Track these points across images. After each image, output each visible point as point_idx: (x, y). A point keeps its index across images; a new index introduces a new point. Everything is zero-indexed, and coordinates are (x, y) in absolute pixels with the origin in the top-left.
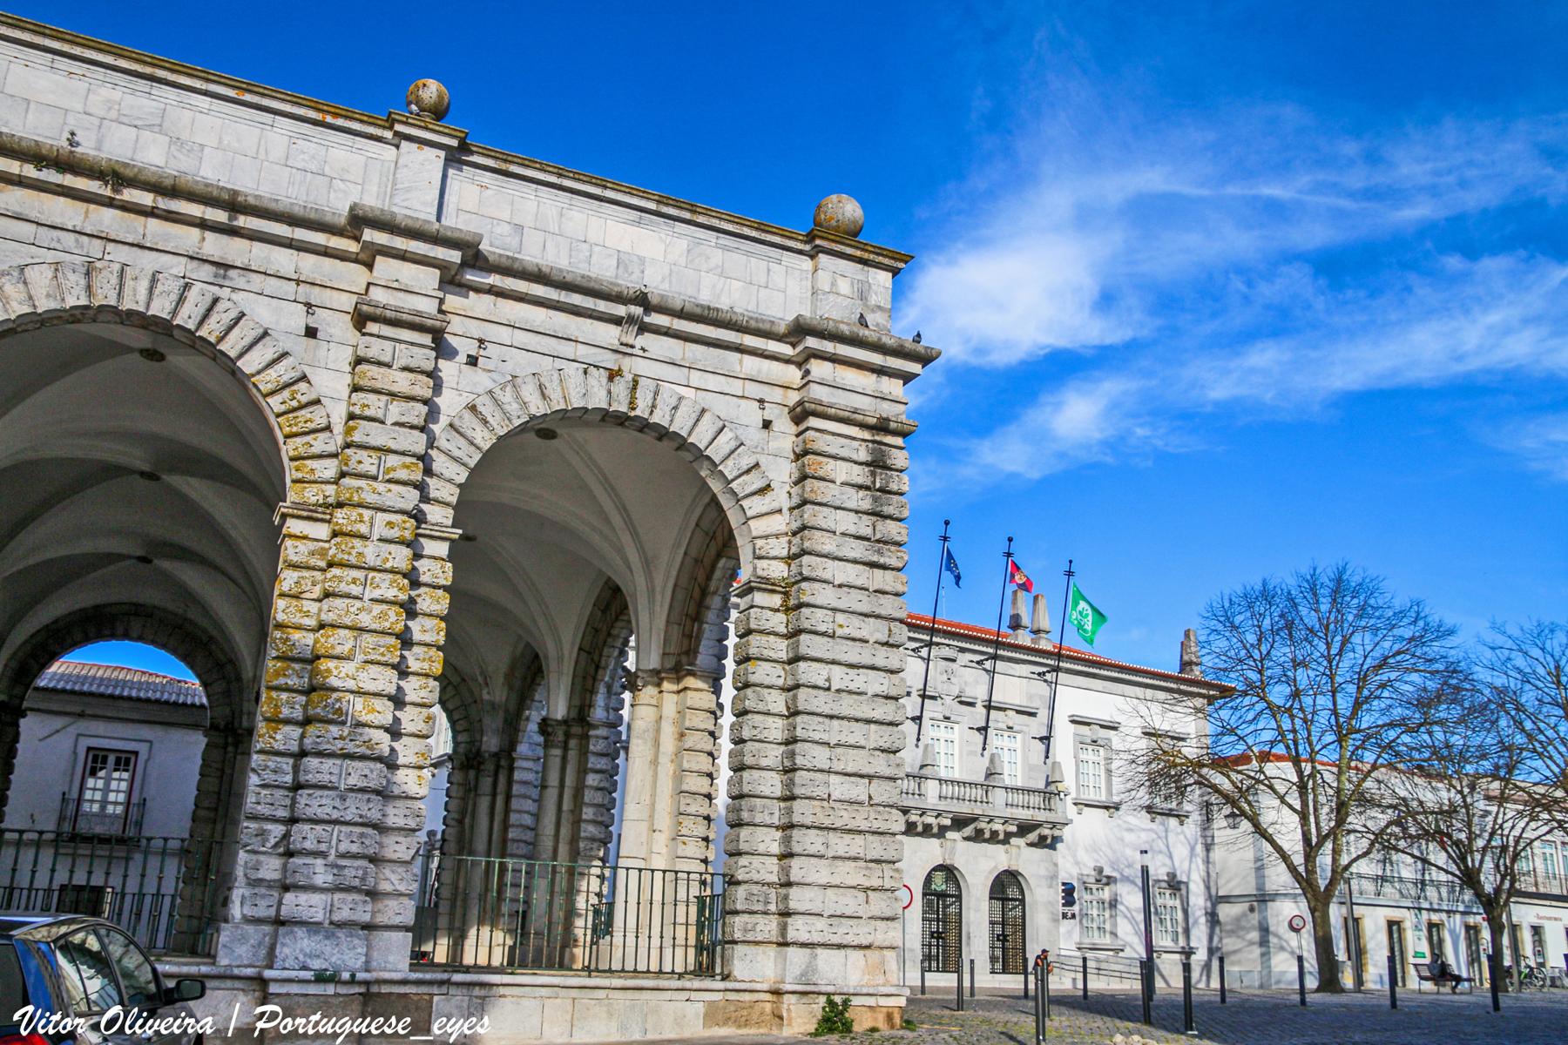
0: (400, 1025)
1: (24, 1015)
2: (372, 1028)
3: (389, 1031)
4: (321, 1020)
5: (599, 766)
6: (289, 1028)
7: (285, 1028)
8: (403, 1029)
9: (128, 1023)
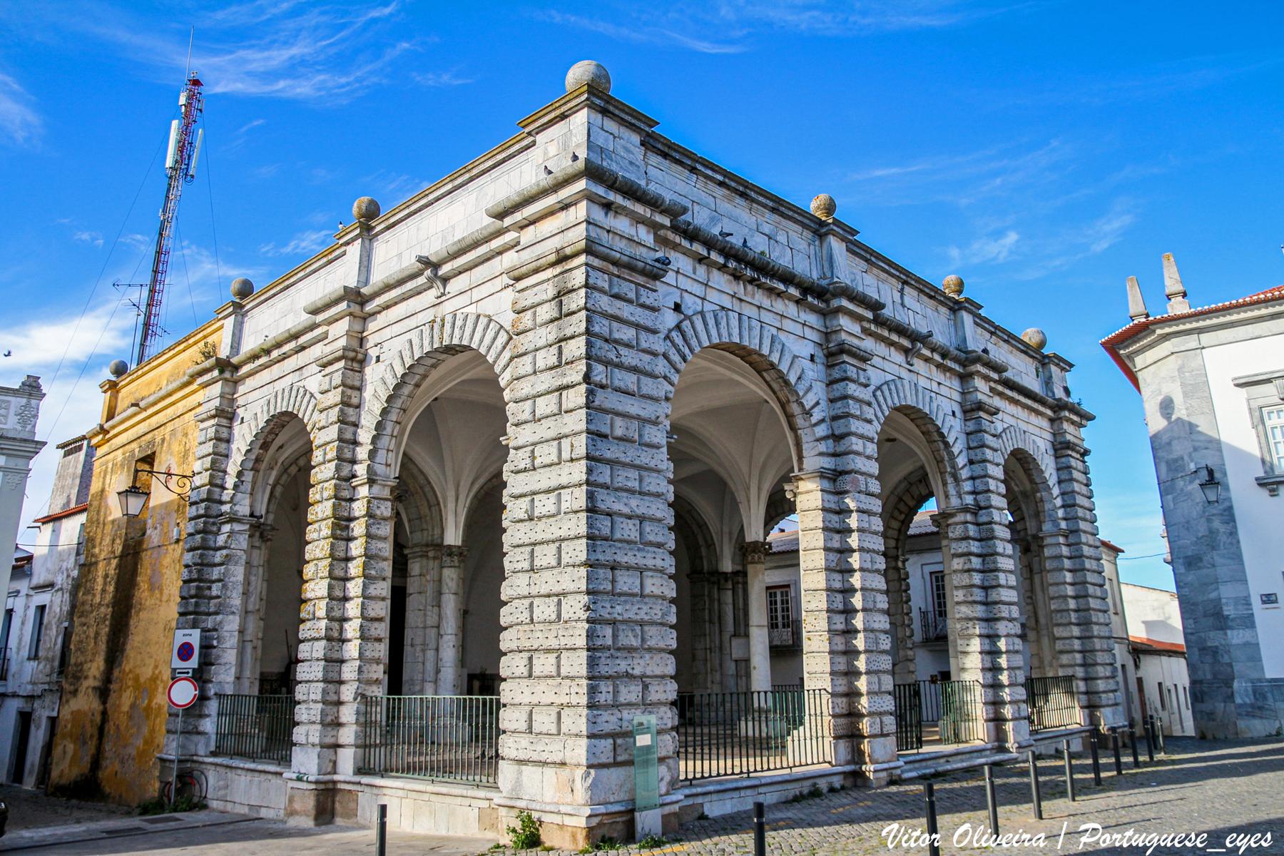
0: (1199, 840)
1: (889, 833)
2: (1252, 842)
3: (1189, 845)
4: (1133, 835)
5: (960, 551)
6: (1108, 842)
7: (1104, 842)
8: (1201, 843)
9: (976, 838)
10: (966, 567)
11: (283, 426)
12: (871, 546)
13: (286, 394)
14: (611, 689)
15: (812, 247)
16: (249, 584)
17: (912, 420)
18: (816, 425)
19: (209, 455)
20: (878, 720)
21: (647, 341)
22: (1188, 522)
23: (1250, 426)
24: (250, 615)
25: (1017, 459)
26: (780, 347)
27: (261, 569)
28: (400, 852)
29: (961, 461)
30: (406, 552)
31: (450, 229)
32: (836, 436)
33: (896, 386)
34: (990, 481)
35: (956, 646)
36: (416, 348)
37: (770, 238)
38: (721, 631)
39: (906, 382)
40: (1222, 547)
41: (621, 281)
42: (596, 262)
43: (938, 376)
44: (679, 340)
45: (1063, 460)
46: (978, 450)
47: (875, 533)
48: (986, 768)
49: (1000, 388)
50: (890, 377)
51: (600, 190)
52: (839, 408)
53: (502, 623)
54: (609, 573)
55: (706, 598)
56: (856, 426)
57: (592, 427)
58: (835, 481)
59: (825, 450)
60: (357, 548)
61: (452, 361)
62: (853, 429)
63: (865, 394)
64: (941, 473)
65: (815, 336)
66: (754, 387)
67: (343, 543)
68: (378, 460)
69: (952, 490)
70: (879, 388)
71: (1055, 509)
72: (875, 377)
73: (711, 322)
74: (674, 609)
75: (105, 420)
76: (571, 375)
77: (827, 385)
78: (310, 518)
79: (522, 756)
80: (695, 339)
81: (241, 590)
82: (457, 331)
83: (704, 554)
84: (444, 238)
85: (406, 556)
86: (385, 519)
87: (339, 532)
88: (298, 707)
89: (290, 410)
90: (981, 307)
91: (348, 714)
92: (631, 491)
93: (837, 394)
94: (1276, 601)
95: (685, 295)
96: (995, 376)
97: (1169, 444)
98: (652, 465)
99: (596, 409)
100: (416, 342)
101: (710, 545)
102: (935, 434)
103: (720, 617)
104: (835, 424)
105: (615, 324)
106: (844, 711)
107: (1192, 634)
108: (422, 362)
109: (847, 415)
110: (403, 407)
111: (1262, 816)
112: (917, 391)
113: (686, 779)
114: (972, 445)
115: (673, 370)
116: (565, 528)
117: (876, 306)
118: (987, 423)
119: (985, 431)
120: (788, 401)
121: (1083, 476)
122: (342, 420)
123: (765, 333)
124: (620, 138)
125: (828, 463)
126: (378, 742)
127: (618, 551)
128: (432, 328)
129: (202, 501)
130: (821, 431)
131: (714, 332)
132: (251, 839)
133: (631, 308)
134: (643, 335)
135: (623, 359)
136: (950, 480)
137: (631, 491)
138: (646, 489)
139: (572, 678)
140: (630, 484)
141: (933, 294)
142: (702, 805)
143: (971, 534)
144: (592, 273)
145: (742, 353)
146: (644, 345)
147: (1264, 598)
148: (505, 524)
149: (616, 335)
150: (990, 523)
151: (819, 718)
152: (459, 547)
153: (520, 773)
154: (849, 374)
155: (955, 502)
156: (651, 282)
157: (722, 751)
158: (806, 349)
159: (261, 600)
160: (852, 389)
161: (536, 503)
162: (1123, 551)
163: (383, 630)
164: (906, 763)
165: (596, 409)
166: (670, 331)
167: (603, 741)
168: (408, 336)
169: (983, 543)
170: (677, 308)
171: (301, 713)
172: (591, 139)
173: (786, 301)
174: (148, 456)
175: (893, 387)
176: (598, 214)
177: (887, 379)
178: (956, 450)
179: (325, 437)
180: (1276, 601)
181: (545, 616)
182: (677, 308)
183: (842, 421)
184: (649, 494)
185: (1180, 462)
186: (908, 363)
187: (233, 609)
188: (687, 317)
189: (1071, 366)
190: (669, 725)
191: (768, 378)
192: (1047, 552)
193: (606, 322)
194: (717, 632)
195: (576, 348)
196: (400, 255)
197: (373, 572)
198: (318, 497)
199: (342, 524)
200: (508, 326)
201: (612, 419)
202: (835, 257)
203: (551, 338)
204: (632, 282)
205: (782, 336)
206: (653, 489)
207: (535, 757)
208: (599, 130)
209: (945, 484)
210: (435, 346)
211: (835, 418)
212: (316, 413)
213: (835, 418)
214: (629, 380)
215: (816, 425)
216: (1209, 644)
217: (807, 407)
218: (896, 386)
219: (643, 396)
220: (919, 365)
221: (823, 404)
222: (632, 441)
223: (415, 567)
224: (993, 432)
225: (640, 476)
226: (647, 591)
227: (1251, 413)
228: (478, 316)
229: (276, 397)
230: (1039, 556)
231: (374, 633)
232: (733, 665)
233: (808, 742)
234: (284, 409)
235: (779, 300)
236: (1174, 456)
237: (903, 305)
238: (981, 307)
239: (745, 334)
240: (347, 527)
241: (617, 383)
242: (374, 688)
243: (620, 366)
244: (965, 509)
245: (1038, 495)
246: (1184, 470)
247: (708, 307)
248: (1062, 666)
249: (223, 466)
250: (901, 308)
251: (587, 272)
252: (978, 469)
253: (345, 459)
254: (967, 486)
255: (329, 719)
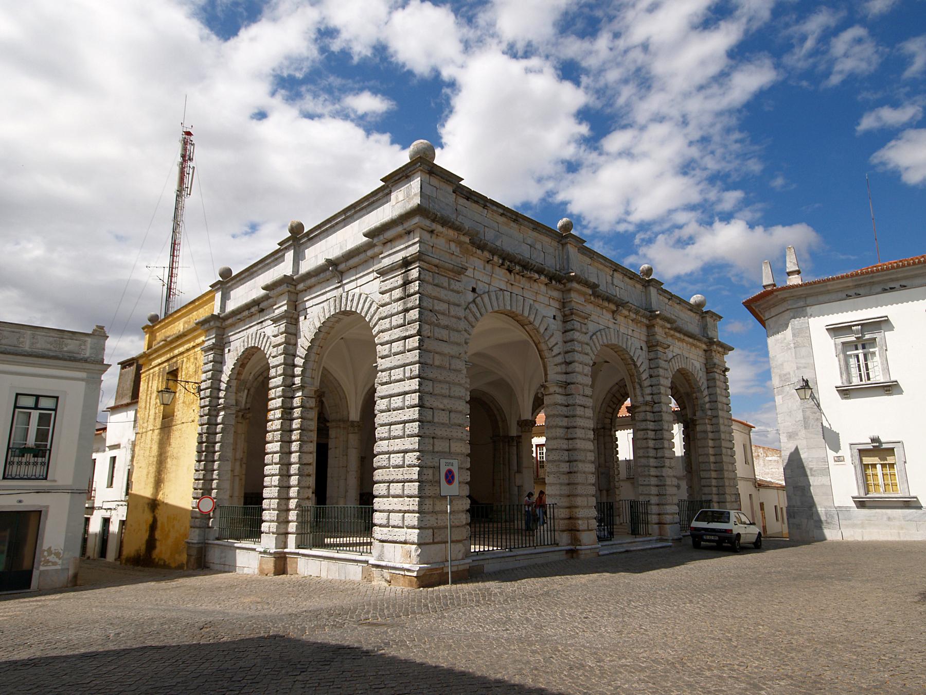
10: (645, 437)
11: (253, 355)
12: (586, 425)
13: (254, 336)
14: (431, 503)
15: (557, 251)
16: (236, 444)
17: (616, 352)
18: (554, 356)
19: (210, 371)
20: (586, 522)
21: (454, 311)
22: (790, 412)
23: (835, 355)
25: (682, 374)
26: (535, 311)
27: (243, 436)
29: (644, 376)
30: (328, 424)
31: (344, 242)
32: (567, 363)
33: (605, 332)
34: (661, 387)
35: (638, 482)
36: (326, 311)
37: (531, 247)
39: (612, 330)
40: (811, 428)
41: (439, 276)
42: (425, 265)
43: (632, 325)
44: (474, 309)
45: (711, 374)
46: (655, 370)
47: (589, 418)
49: (672, 332)
50: (602, 327)
51: (427, 223)
52: (569, 347)
53: (374, 466)
54: (431, 440)
56: (577, 357)
57: (422, 361)
58: (565, 388)
59: (560, 371)
60: (296, 424)
61: (346, 319)
62: (576, 359)
63: (585, 339)
64: (632, 382)
65: (556, 305)
66: (519, 334)
67: (288, 422)
68: (307, 375)
69: (638, 392)
70: (594, 334)
71: (705, 404)
72: (592, 327)
73: (494, 298)
74: (469, 459)
75: (146, 348)
76: (411, 330)
77: (563, 333)
78: (271, 385)
79: (384, 538)
80: (484, 308)
81: (232, 448)
82: (349, 302)
83: (500, 426)
84: (341, 248)
85: (328, 427)
86: (311, 408)
87: (285, 416)
88: (264, 512)
89: (256, 345)
90: (663, 284)
91: (293, 515)
92: (444, 396)
93: (568, 338)
94: (843, 460)
95: (479, 282)
96: (669, 326)
97: (782, 365)
98: (456, 381)
99: (425, 350)
100: (326, 308)
101: (504, 420)
102: (629, 360)
103: (509, 463)
104: (567, 356)
105: (436, 301)
106: (567, 517)
107: (789, 478)
108: (329, 320)
109: (573, 351)
110: (321, 345)
112: (618, 335)
113: (475, 551)
114: (652, 367)
115: (470, 327)
116: (408, 415)
117: (594, 287)
118: (662, 354)
119: (660, 358)
120: (539, 343)
121: (724, 384)
122: (285, 352)
123: (526, 304)
124: (440, 189)
125: (563, 378)
126: (309, 531)
127: (436, 428)
128: (335, 301)
129: (208, 397)
130: (559, 359)
131: (495, 304)
132: (287, 239)
133: (446, 292)
134: (452, 308)
135: (440, 321)
136: (637, 386)
137: (444, 396)
138: (452, 394)
139: (411, 497)
140: (443, 391)
141: (632, 277)
142: (483, 566)
143: (649, 418)
144: (422, 272)
145: (513, 315)
146: (452, 313)
147: (836, 459)
148: (376, 412)
149: (436, 308)
150: (660, 412)
151: (552, 521)
152: (358, 422)
153: (383, 547)
154: (575, 326)
155: (640, 399)
156: (458, 276)
157: (491, 536)
158: (551, 312)
159: (244, 452)
160: (577, 335)
161: (392, 401)
162: (754, 428)
163: (312, 470)
164: (602, 546)
165: (425, 350)
166: (469, 304)
167: (427, 530)
168: (322, 305)
169: (656, 423)
170: (474, 290)
171: (266, 515)
172: (423, 190)
173: (540, 284)
174: (175, 370)
175: (603, 333)
176: (427, 236)
177: (600, 328)
178: (641, 370)
179: (276, 360)
180: (843, 460)
181: (396, 463)
182: (474, 290)
183: (571, 353)
184: (455, 397)
185: (788, 376)
186: (614, 319)
188: (480, 295)
189: (722, 317)
190: (464, 523)
191: (528, 329)
192: (698, 428)
193: (431, 300)
194: (507, 470)
195: (414, 314)
196: (316, 256)
197: (305, 438)
198: (273, 396)
199: (287, 411)
200: (377, 301)
201: (433, 355)
202: (570, 256)
203: (400, 308)
204: (446, 276)
205: (537, 305)
206: (457, 394)
207: (391, 538)
208: (427, 185)
209: (634, 389)
210: (337, 311)
211: (566, 352)
212: (271, 347)
213: (566, 352)
214: (444, 334)
215: (554, 356)
216: (799, 484)
217: (550, 346)
218: (605, 332)
219: (452, 343)
220: (620, 319)
221: (560, 344)
222: (445, 368)
223: (332, 433)
224: (665, 359)
225: (449, 387)
226: (453, 450)
227: (836, 347)
228: (361, 295)
229: (248, 337)
230: (693, 430)
231: (306, 472)
233: (546, 532)
234: (253, 345)
235: (536, 284)
236: (784, 372)
237: (613, 284)
238: (663, 284)
239: (514, 304)
240: (290, 413)
241: (436, 335)
242: (307, 502)
243: (438, 326)
244: (646, 404)
245: (694, 395)
246: (790, 381)
247: (492, 288)
248: (705, 494)
249: (219, 377)
250: (611, 285)
251: (419, 271)
252: (654, 381)
253: (288, 375)
254: (648, 390)
255: (281, 519)
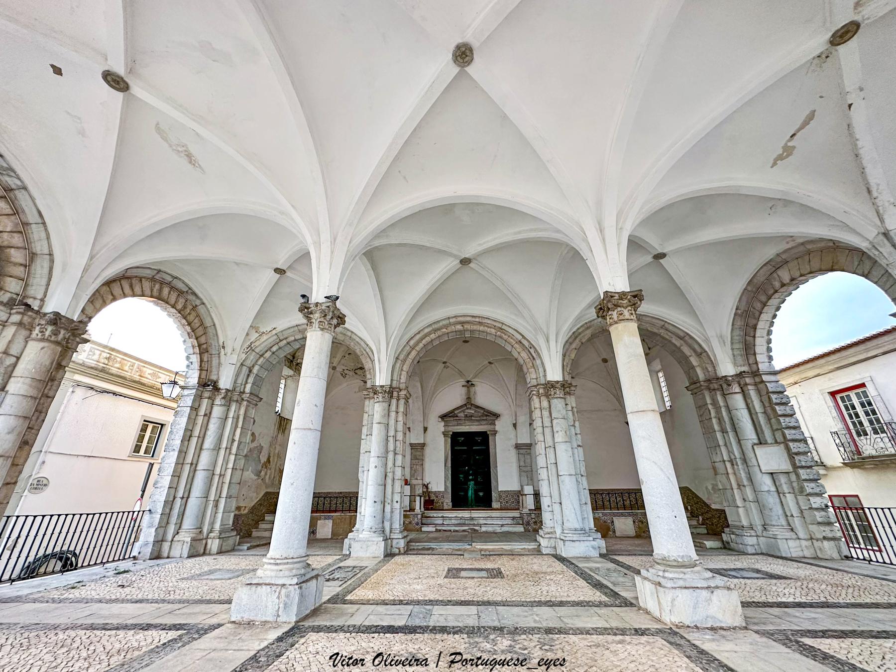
24: (754, 362)
28: (103, 670)
38: (739, 441)
48: (644, 511)
55: (710, 407)
101: (701, 353)
111: (545, 502)
187: (174, 448)
232: (767, 480)
